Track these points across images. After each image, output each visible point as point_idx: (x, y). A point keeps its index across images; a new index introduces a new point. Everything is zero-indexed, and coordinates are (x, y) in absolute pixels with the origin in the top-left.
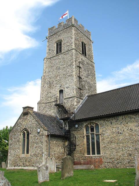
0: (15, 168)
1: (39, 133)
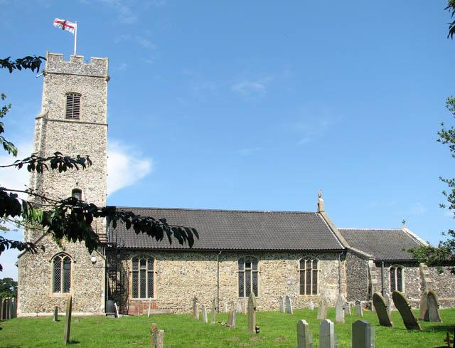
0: (39, 314)
1: (94, 263)
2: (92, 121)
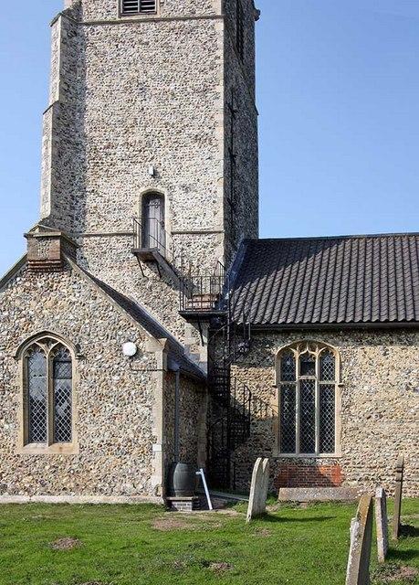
2: (186, 12)
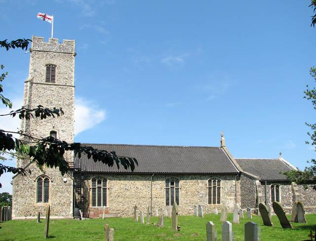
0: (27, 218)
2: (64, 84)
